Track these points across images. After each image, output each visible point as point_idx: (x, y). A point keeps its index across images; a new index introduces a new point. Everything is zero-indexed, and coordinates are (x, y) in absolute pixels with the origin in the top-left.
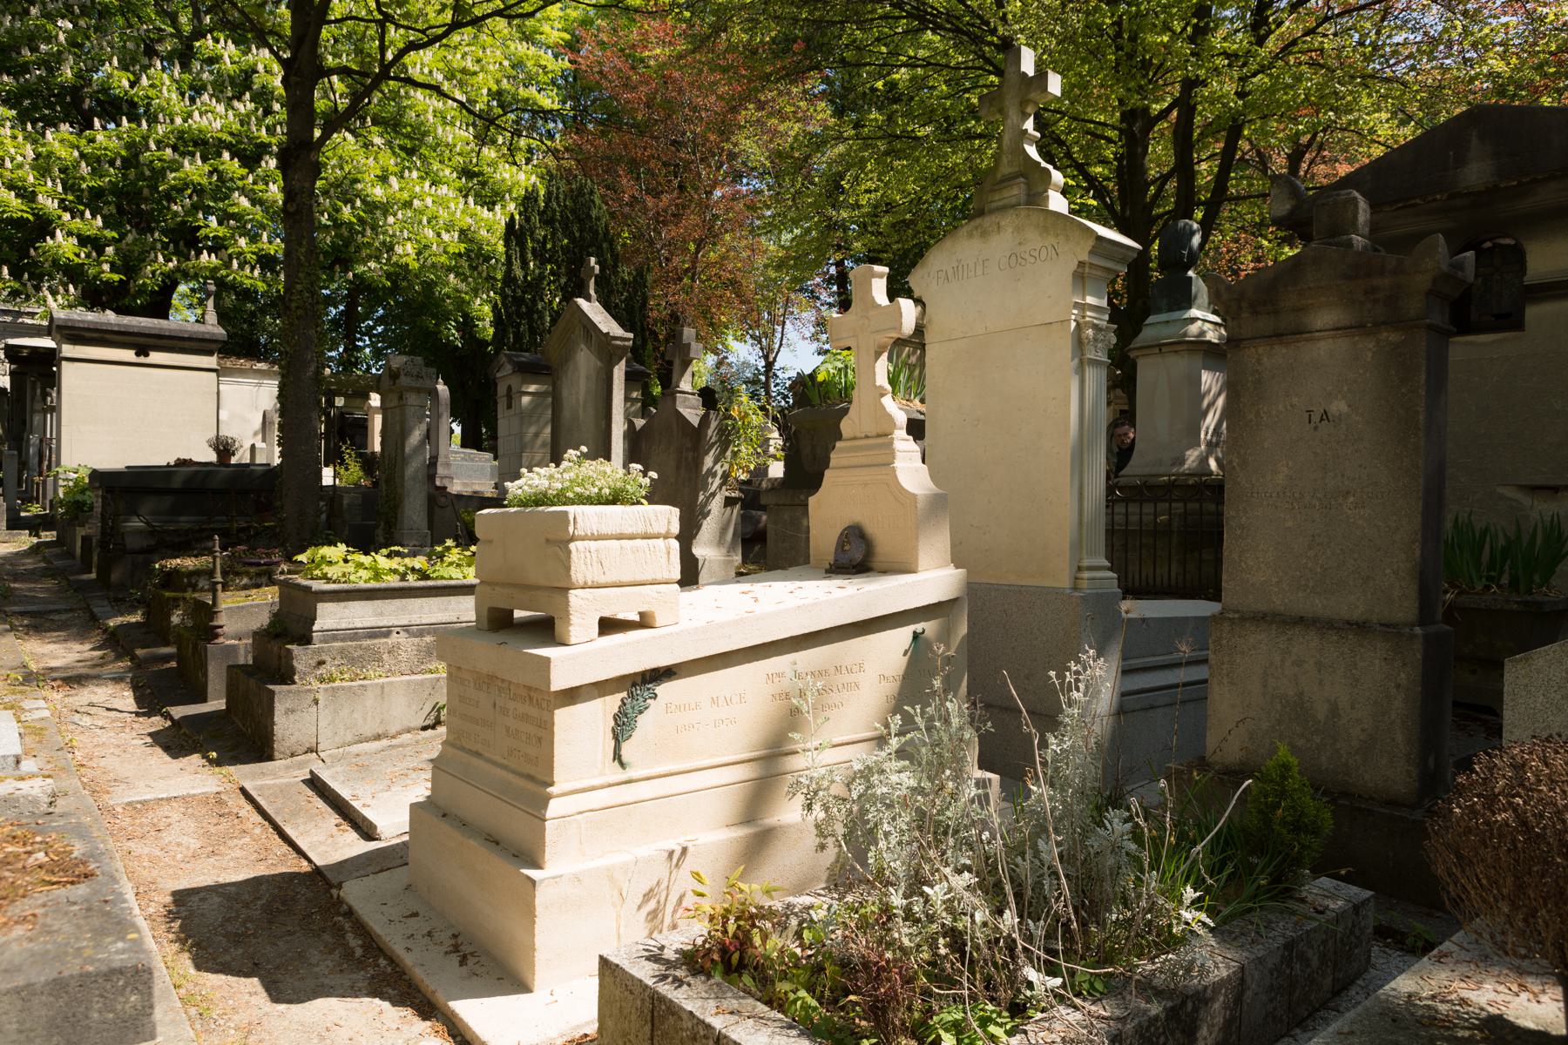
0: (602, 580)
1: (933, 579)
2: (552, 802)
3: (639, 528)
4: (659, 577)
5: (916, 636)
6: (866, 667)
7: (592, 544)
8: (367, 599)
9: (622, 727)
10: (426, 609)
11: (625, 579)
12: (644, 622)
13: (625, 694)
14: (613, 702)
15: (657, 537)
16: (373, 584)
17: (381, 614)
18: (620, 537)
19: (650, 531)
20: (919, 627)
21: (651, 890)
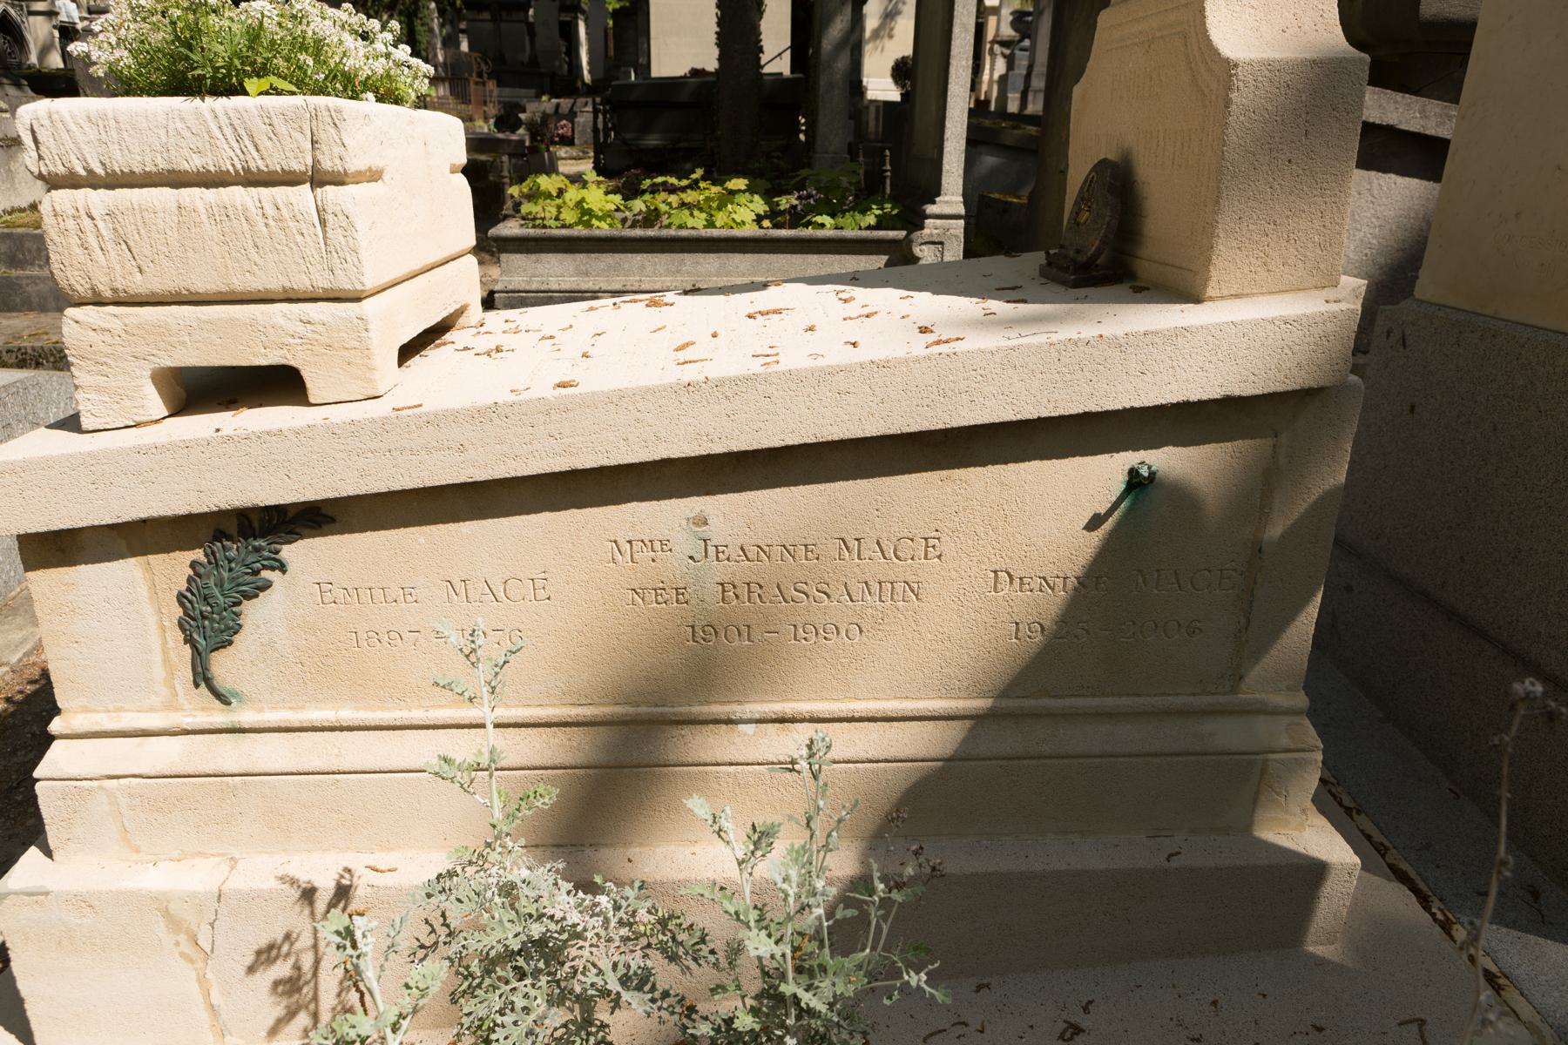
0: (138, 284)
1: (1254, 316)
2: (56, 745)
3: (227, 158)
4: (301, 283)
5: (1137, 483)
6: (947, 545)
7: (97, 199)
8: (528, 251)
9: (208, 625)
10: (649, 269)
11: (203, 283)
12: (279, 384)
13: (198, 555)
14: (176, 567)
15: (289, 179)
16: (580, 231)
17: (587, 274)
18: (177, 180)
19: (257, 163)
20: (1165, 460)
21: (271, 947)
